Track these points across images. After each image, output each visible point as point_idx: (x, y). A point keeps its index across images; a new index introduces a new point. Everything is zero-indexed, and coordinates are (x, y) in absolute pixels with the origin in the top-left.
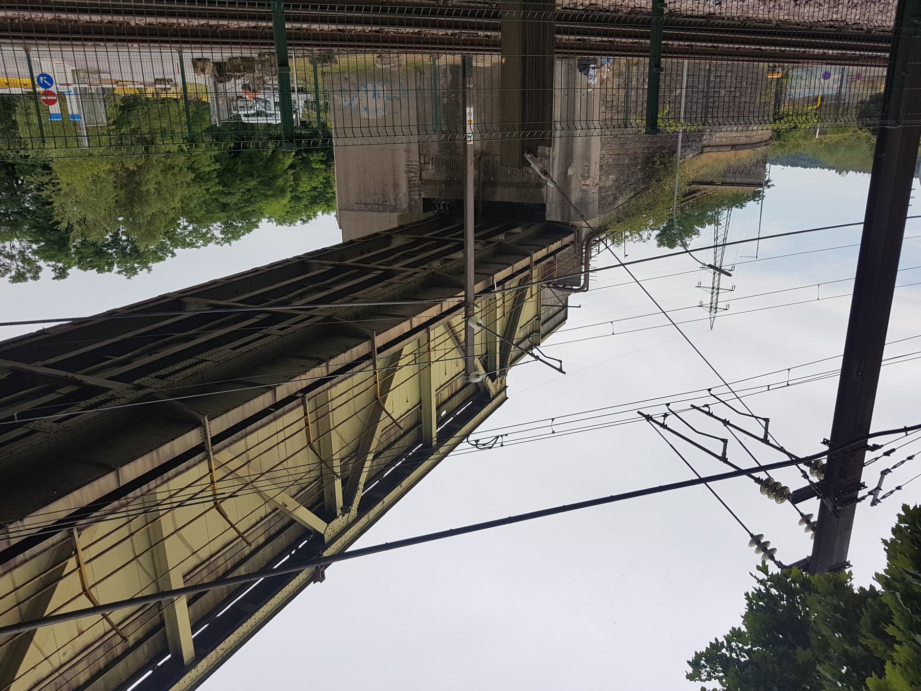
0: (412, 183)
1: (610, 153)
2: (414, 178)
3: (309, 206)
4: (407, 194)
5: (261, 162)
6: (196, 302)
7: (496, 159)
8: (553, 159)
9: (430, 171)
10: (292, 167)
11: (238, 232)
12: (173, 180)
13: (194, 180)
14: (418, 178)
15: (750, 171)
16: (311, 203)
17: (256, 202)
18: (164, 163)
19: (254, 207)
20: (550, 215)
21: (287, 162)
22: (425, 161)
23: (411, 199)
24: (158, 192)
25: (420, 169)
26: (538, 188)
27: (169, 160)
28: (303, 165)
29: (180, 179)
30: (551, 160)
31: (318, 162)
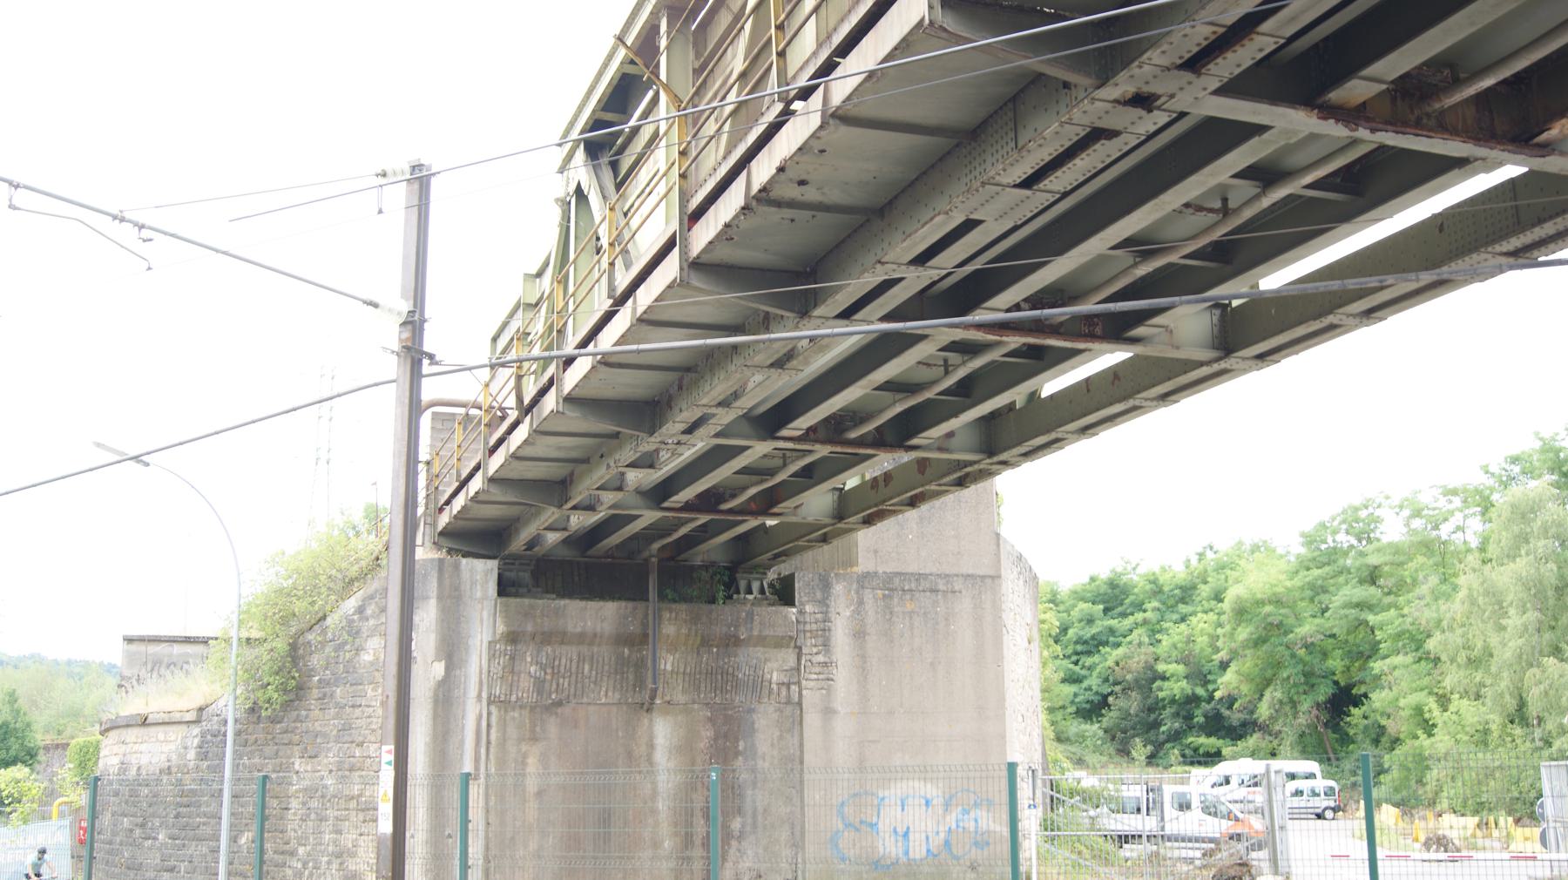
0: (820, 641)
1: (371, 709)
2: (815, 650)
3: (1197, 581)
4: (832, 616)
5: (1285, 675)
6: (1178, 348)
7: (617, 696)
8: (479, 697)
9: (776, 667)
10: (1224, 666)
11: (1344, 522)
12: (1470, 636)
13: (1429, 636)
14: (805, 651)
15: (152, 670)
16: (1194, 587)
17: (1302, 589)
18: (1488, 671)
19: (1306, 577)
20: (486, 573)
21: (1235, 676)
22: (789, 688)
23: (824, 602)
24: (1503, 608)
25: (798, 670)
26: (513, 632)
27: (1478, 679)
28: (1205, 670)
29: (1456, 638)
30: (485, 695)
31: (1172, 675)
